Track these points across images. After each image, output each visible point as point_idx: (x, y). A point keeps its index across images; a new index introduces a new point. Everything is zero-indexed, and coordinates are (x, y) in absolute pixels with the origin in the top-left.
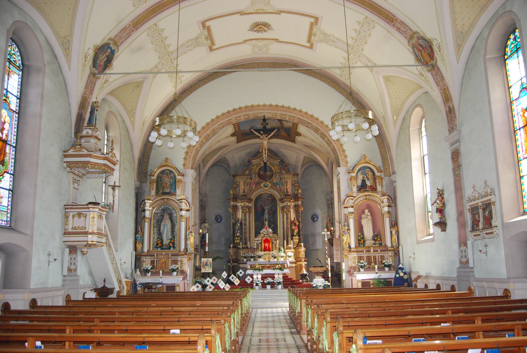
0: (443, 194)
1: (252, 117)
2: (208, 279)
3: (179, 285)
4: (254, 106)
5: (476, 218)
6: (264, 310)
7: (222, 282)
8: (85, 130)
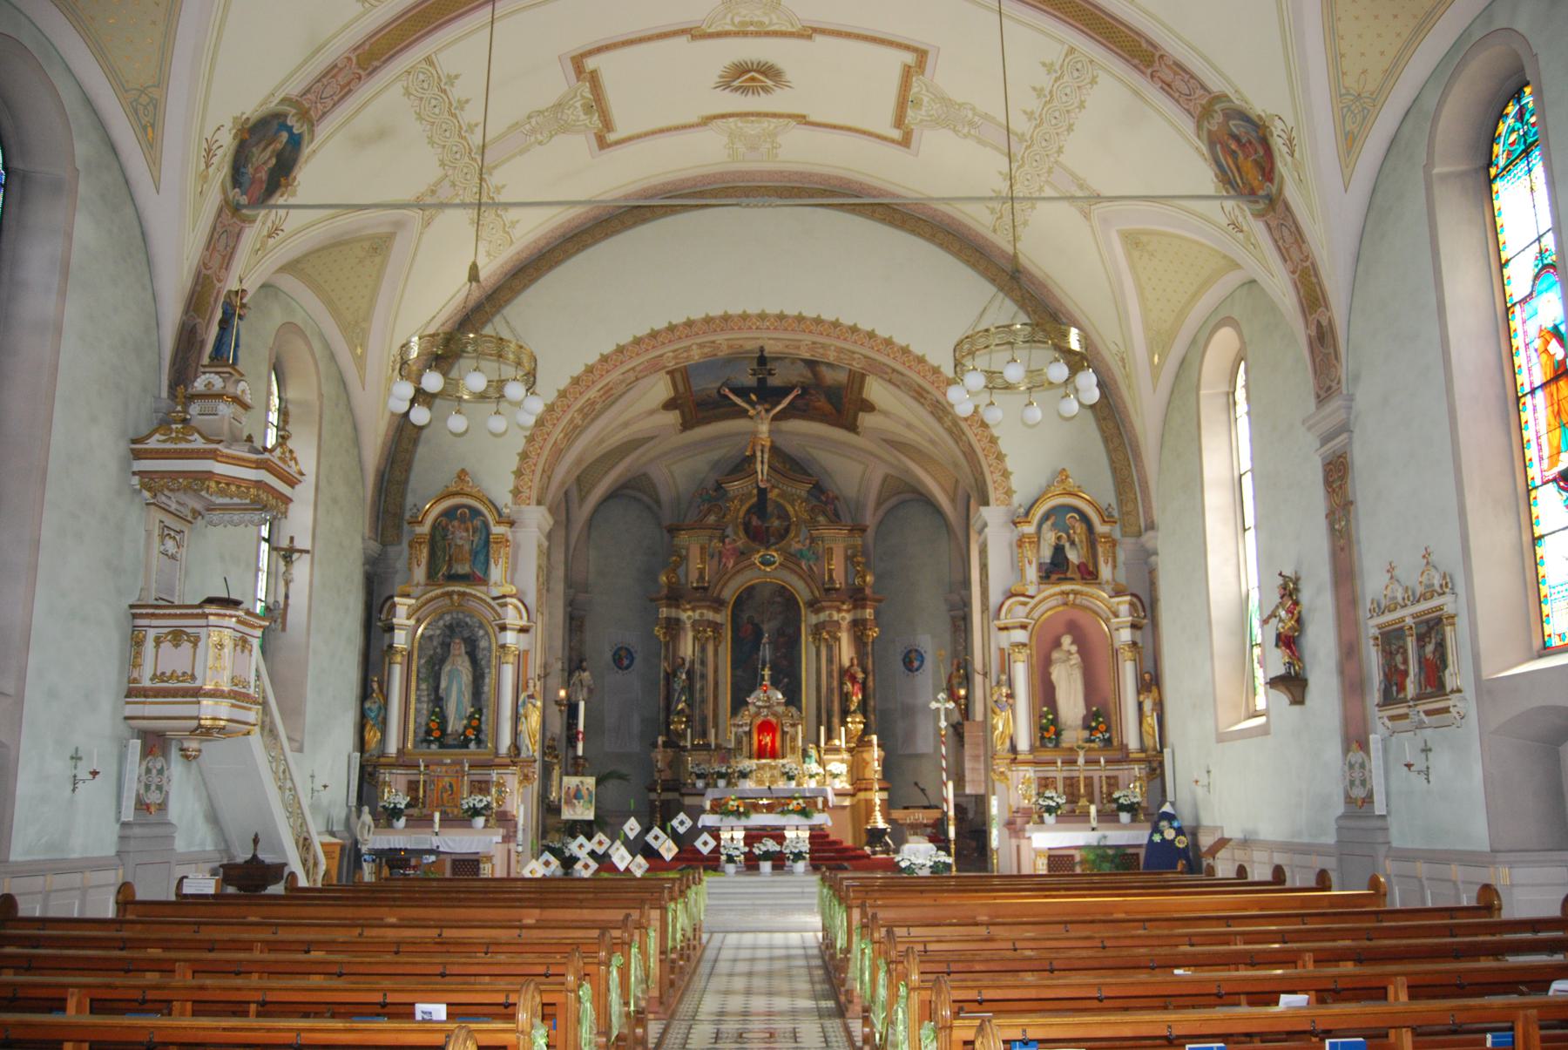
0: (1296, 590)
1: (724, 352)
2: (581, 839)
3: (489, 858)
4: (730, 316)
5: (1396, 665)
6: (748, 939)
7: (623, 851)
8: (203, 377)
